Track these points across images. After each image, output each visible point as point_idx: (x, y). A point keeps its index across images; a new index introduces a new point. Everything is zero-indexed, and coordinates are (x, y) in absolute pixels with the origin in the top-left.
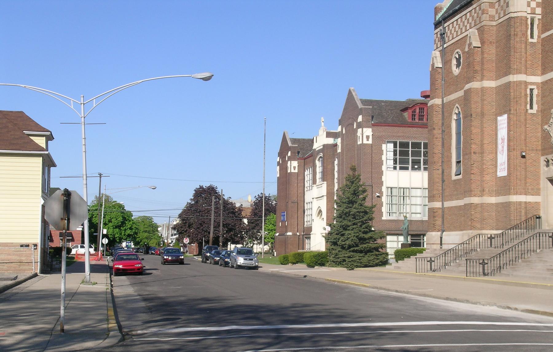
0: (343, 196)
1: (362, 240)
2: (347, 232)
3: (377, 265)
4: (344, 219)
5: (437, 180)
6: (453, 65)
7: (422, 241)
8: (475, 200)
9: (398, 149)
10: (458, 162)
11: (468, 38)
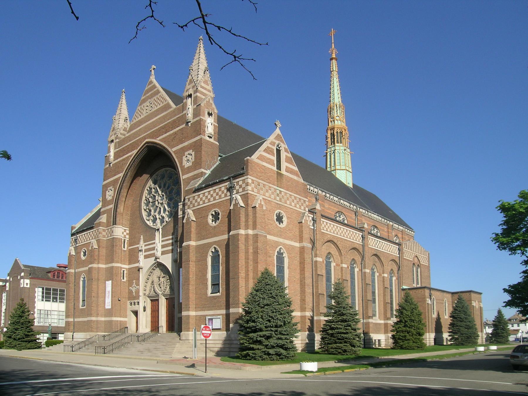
0: (15, 313)
1: (27, 336)
2: (18, 332)
3: (36, 348)
4: (16, 325)
5: (71, 308)
6: (81, 255)
7: (57, 336)
8: (94, 319)
9: (45, 291)
10: (84, 300)
11: (91, 244)
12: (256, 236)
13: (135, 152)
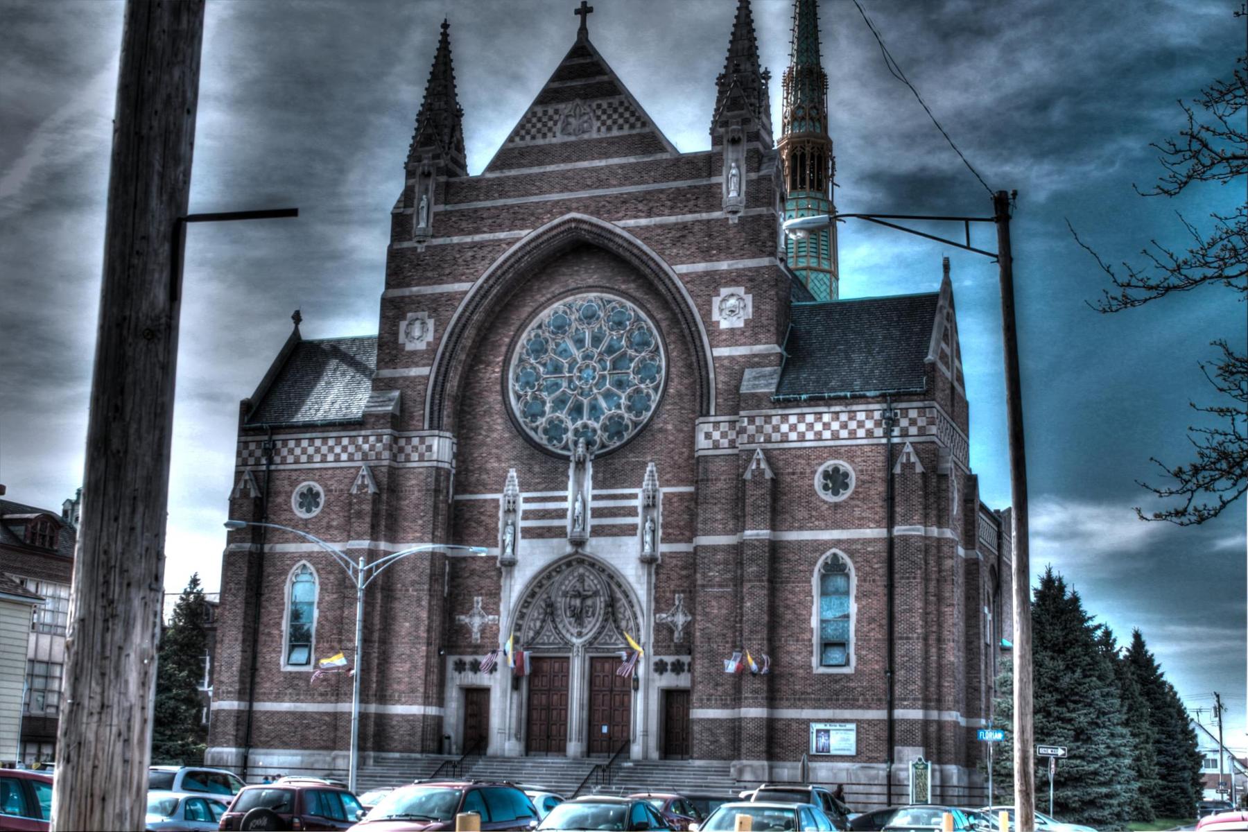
12: (775, 550)
13: (526, 235)
